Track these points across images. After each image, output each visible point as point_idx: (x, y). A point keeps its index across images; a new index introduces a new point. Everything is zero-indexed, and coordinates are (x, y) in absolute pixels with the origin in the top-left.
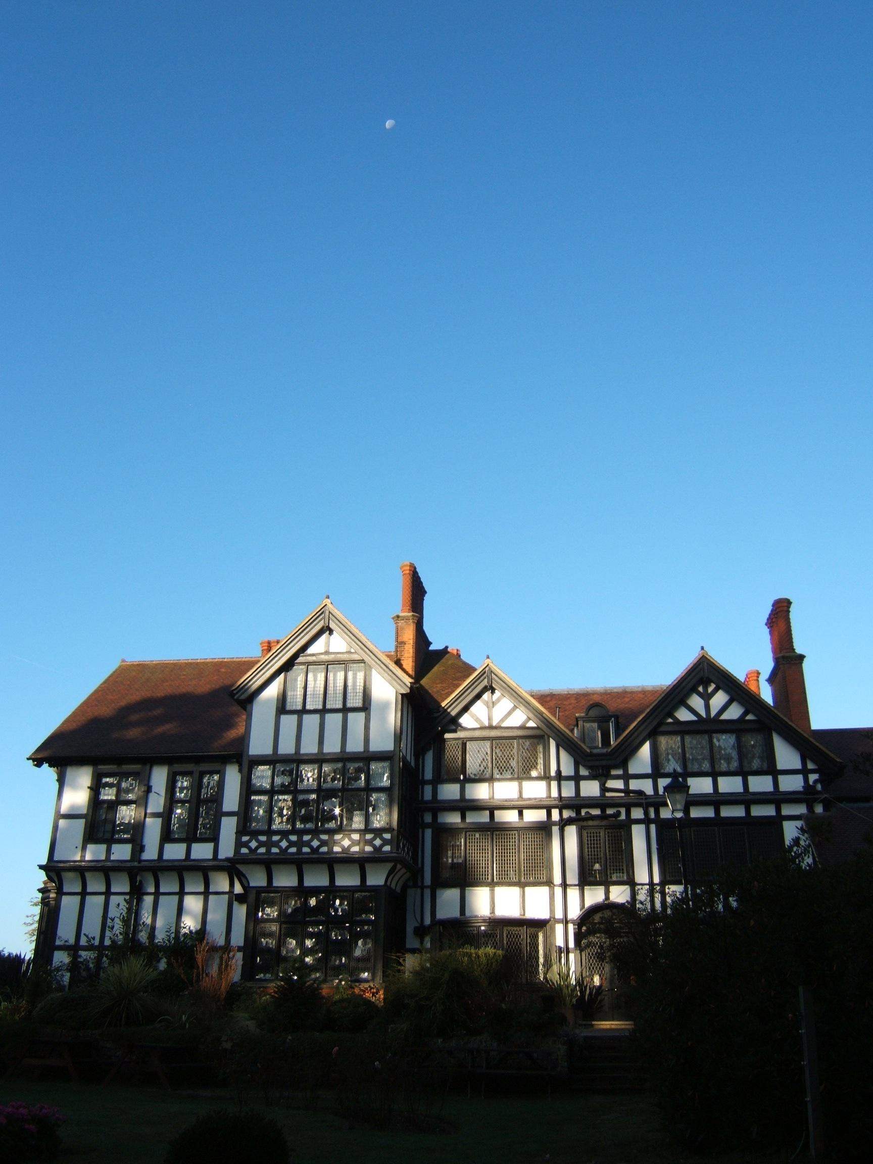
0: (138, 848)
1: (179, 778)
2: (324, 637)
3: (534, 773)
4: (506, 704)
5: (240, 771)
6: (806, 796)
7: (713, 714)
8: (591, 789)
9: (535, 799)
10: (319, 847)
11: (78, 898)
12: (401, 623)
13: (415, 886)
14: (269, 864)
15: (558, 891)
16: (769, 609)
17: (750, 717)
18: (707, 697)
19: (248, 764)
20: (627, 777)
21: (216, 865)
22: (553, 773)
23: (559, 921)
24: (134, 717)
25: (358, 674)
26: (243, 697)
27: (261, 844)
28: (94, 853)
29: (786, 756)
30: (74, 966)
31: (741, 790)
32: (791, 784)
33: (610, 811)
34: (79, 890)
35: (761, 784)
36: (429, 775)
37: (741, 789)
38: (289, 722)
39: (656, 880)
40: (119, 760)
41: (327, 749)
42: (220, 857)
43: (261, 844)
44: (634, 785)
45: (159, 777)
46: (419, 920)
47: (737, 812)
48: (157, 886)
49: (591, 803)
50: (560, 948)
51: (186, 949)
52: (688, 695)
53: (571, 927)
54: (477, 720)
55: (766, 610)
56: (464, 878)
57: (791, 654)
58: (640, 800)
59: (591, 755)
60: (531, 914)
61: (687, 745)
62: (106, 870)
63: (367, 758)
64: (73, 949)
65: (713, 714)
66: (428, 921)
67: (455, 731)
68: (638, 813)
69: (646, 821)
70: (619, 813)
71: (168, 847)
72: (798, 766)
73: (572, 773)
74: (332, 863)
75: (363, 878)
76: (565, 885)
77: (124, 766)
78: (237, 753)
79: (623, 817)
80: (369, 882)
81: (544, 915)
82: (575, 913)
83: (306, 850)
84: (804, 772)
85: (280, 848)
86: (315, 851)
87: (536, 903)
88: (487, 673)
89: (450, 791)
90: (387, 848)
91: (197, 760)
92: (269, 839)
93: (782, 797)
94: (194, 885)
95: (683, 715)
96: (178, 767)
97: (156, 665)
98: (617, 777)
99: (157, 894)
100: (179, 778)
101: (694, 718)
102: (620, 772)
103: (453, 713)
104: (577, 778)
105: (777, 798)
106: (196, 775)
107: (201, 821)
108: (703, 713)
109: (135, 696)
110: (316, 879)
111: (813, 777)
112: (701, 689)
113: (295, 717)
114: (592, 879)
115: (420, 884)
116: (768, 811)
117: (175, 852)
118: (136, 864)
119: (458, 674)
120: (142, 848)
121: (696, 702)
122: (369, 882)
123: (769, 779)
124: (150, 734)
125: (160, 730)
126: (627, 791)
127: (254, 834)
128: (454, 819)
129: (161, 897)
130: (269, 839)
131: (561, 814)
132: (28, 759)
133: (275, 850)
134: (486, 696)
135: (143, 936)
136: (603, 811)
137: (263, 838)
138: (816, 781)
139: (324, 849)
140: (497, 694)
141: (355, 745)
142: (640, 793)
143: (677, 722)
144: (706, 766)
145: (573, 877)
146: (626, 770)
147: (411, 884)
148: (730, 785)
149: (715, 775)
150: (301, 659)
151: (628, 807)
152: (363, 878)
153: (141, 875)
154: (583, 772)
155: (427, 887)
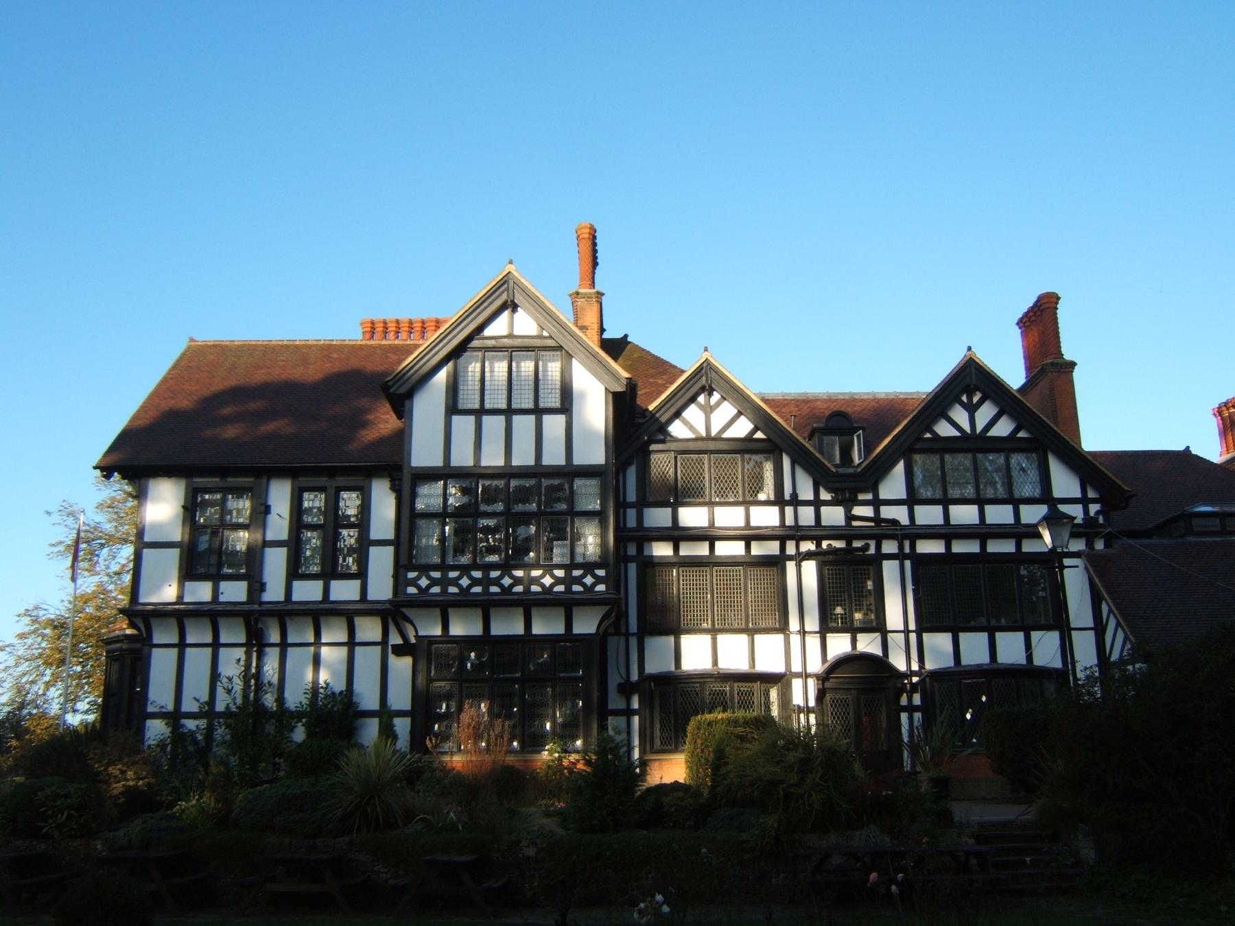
0: (258, 586)
1: (306, 495)
3: (762, 497)
4: (727, 410)
5: (393, 488)
6: (1087, 530)
7: (979, 429)
8: (834, 515)
9: (766, 527)
10: (512, 586)
11: (209, 650)
12: (581, 302)
13: (617, 633)
14: (444, 608)
15: (795, 640)
16: (1029, 302)
17: (1022, 434)
18: (972, 409)
19: (407, 481)
21: (366, 608)
22: (787, 497)
23: (798, 675)
24: (227, 411)
25: (496, 365)
26: (402, 390)
27: (434, 582)
28: (201, 592)
30: (179, 736)
31: (941, 522)
33: (857, 544)
36: (632, 496)
38: (463, 426)
39: (912, 626)
40: (223, 472)
41: (547, 461)
42: (370, 598)
43: (434, 582)
44: (887, 512)
45: (280, 495)
46: (624, 674)
47: (972, 547)
48: (284, 635)
49: (834, 533)
50: (799, 707)
51: (335, 715)
52: (949, 406)
53: (811, 683)
54: (691, 428)
55: (1027, 302)
56: (666, 621)
57: (1060, 361)
58: (890, 529)
60: (762, 667)
61: (948, 467)
62: (213, 614)
63: (571, 472)
64: (174, 717)
65: (979, 429)
66: (635, 677)
67: (663, 442)
68: (889, 547)
69: (900, 556)
70: (867, 547)
71: (297, 585)
72: (1077, 494)
74: (529, 604)
75: (569, 625)
76: (803, 632)
77: (229, 479)
78: (391, 462)
79: (872, 551)
80: (577, 630)
81: (779, 668)
82: (815, 665)
83: (494, 589)
84: (1084, 501)
85: (459, 586)
86: (507, 590)
87: (769, 654)
88: (705, 369)
89: (658, 517)
90: (601, 588)
91: (332, 472)
92: (486, 575)
93: (1025, 530)
94: (334, 633)
95: (944, 429)
96: (305, 481)
97: (239, 346)
98: (865, 503)
99: (284, 645)
100: (306, 495)
101: (957, 434)
102: (869, 496)
103: (663, 419)
104: (817, 503)
106: (332, 491)
107: (328, 548)
108: (967, 428)
109: (220, 384)
110: (508, 626)
111: (1094, 508)
112: (964, 398)
113: (472, 418)
114: (834, 625)
115: (623, 631)
117: (308, 591)
118: (256, 607)
119: (652, 371)
120: (262, 587)
121: (960, 415)
122: (577, 630)
124: (244, 436)
125: (269, 427)
126: (877, 519)
127: (425, 569)
128: (662, 550)
129: (289, 649)
131: (797, 547)
132: (95, 468)
133: (453, 589)
134: (701, 399)
135: (269, 700)
136: (849, 543)
137: (436, 575)
138: (1097, 513)
139: (519, 589)
140: (716, 396)
141: (554, 456)
142: (895, 522)
143: (937, 437)
144: (969, 491)
145: (812, 624)
146: (876, 494)
147: (612, 630)
149: (946, 502)
150: (475, 343)
152: (569, 625)
153: (259, 622)
154: (825, 495)
155: (633, 634)
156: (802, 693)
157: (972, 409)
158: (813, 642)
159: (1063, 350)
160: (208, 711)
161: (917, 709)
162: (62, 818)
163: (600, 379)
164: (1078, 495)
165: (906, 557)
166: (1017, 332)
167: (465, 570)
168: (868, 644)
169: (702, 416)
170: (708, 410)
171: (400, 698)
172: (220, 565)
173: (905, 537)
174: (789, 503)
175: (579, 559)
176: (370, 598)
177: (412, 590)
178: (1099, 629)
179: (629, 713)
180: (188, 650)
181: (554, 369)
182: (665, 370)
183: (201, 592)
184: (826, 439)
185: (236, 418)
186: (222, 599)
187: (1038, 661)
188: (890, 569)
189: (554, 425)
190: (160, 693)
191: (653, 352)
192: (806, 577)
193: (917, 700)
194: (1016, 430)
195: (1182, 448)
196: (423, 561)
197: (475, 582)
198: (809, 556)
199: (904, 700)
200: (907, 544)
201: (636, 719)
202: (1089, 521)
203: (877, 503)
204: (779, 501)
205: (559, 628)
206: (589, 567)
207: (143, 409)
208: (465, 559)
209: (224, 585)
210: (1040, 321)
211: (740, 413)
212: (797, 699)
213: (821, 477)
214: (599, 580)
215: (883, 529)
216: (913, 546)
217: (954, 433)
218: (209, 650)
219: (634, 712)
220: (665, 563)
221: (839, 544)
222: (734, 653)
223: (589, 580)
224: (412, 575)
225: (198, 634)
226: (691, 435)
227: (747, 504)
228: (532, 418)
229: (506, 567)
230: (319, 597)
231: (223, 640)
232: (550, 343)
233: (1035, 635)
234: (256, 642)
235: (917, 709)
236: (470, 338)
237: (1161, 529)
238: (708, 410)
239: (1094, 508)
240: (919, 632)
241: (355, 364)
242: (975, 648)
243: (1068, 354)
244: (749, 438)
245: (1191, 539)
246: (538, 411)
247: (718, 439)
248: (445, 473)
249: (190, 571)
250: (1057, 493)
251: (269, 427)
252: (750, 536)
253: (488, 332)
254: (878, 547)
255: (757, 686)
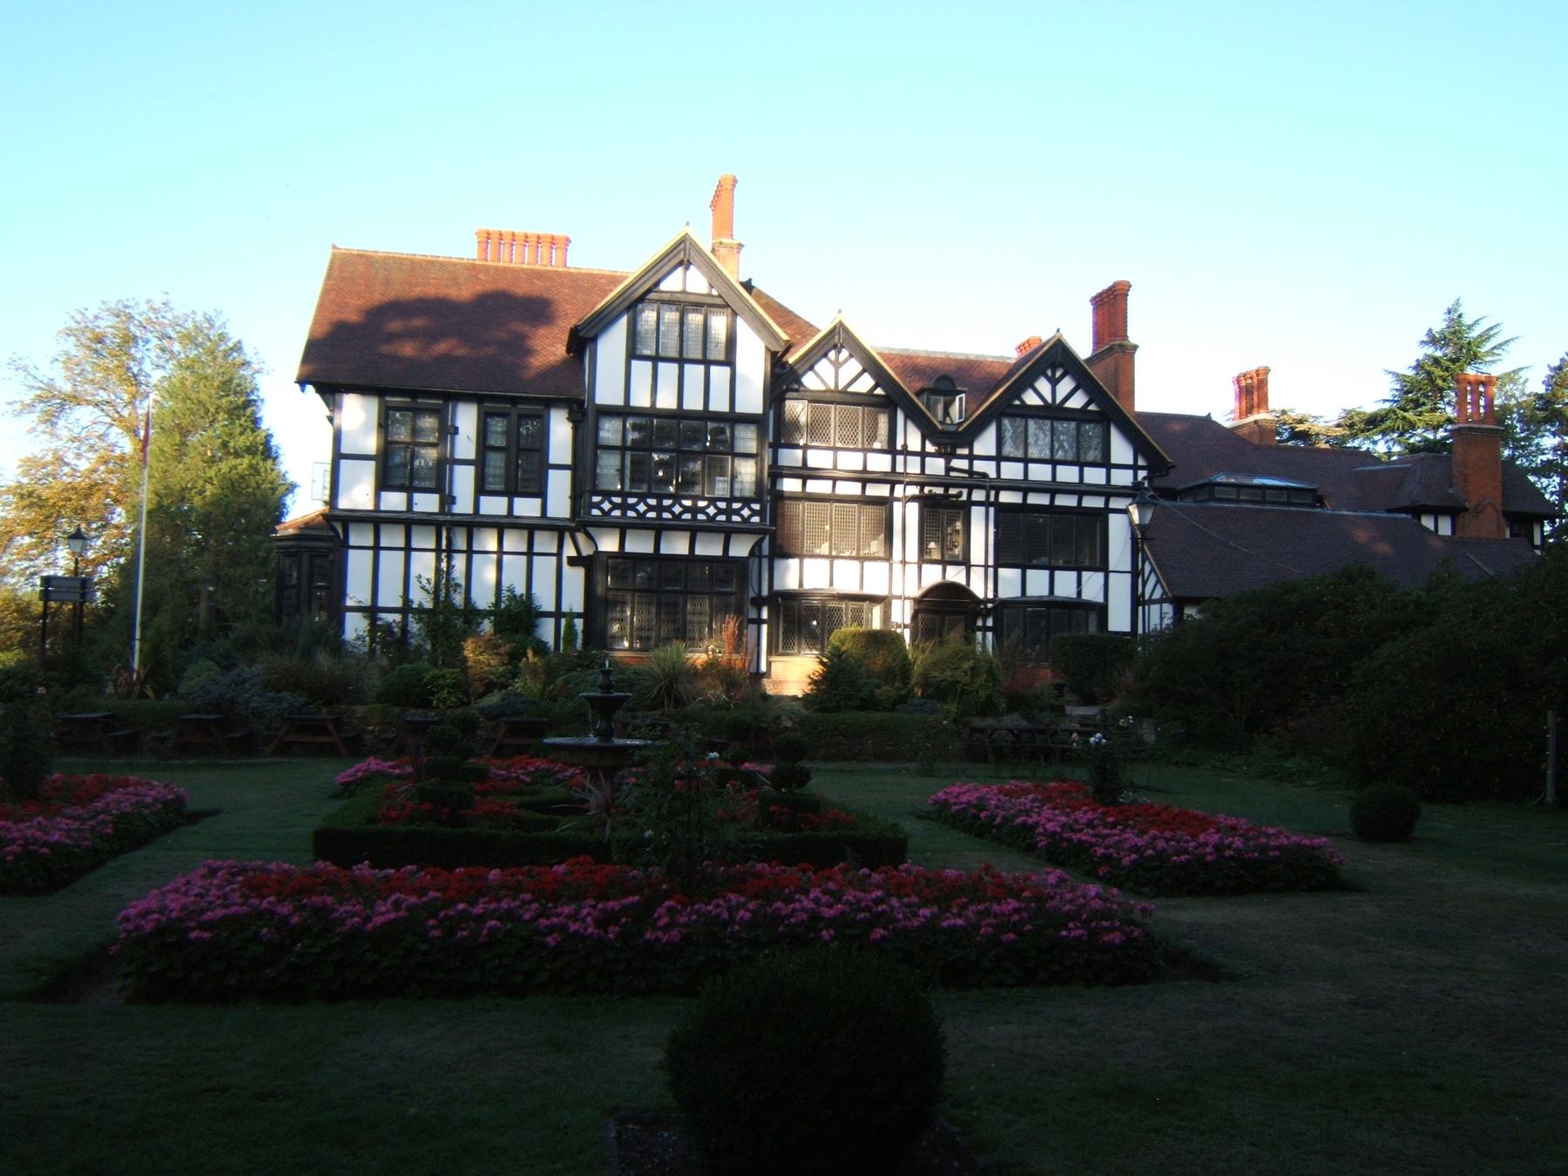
2: (681, 269)
8: (936, 466)
15: (897, 567)
18: (1054, 382)
19: (585, 415)
20: (971, 458)
21: (544, 524)
28: (394, 501)
29: (1121, 450)
32: (1122, 478)
33: (952, 491)
34: (371, 543)
35: (1095, 476)
37: (1103, 482)
39: (991, 562)
40: (414, 394)
44: (979, 466)
45: (466, 419)
47: (1043, 500)
49: (935, 481)
52: (1036, 378)
59: (943, 433)
62: (409, 522)
63: (734, 418)
64: (372, 611)
66: (765, 592)
68: (978, 495)
69: (986, 504)
70: (960, 494)
71: (483, 499)
73: (918, 449)
79: (964, 498)
80: (732, 553)
81: (881, 591)
83: (666, 515)
84: (1135, 468)
87: (875, 579)
90: (756, 519)
92: (625, 501)
95: (1031, 399)
98: (962, 457)
102: (965, 451)
105: (1108, 491)
106: (514, 418)
107: (520, 469)
108: (1049, 400)
110: (677, 545)
111: (1142, 474)
116: (1095, 502)
117: (494, 506)
120: (453, 500)
121: (1043, 385)
123: (1103, 471)
125: (442, 347)
126: (970, 472)
127: (607, 495)
130: (729, 505)
134: (832, 355)
135: (458, 599)
136: (946, 491)
137: (617, 500)
140: (845, 353)
141: (719, 404)
142: (984, 475)
143: (1024, 405)
146: (971, 450)
148: (1068, 474)
150: (652, 296)
151: (971, 488)
154: (930, 448)
156: (902, 614)
157: (1054, 382)
158: (912, 570)
159: (1129, 333)
160: (406, 608)
161: (989, 629)
162: (445, 694)
163: (763, 339)
164: (1131, 462)
165: (991, 504)
166: (1090, 308)
167: (642, 498)
168: (955, 575)
169: (832, 370)
170: (837, 365)
171: (574, 599)
172: (412, 478)
173: (993, 488)
174: (901, 453)
175: (737, 494)
176: (549, 514)
177: (596, 512)
178: (1136, 573)
179: (759, 622)
180: (382, 553)
181: (719, 324)
182: (806, 329)
183: (394, 501)
184: (933, 398)
185: (411, 335)
186: (416, 509)
187: (1086, 596)
188: (977, 513)
189: (720, 374)
190: (357, 591)
191: (778, 299)
192: (908, 516)
193: (990, 623)
194: (1088, 404)
195: (1204, 414)
196: (605, 487)
197: (650, 508)
198: (913, 499)
199: (980, 623)
200: (993, 493)
201: (765, 628)
202: (1137, 485)
203: (971, 458)
204: (891, 450)
205: (717, 551)
206: (746, 502)
207: (316, 322)
208: (644, 489)
209: (417, 497)
210: (1110, 306)
211: (864, 371)
212: (896, 617)
213: (928, 431)
214: (754, 513)
215: (975, 480)
216: (997, 496)
217: (1038, 402)
218: (402, 554)
219: (764, 622)
220: (796, 498)
221: (939, 491)
222: (847, 578)
223: (746, 512)
224: (596, 499)
225: (393, 537)
226: (822, 388)
227: (865, 451)
228: (701, 368)
229: (677, 498)
230: (505, 512)
231: (414, 545)
232: (719, 301)
233: (1085, 575)
234: (445, 551)
235: (989, 629)
236: (649, 291)
237: (1190, 492)
238: (837, 365)
239: (1142, 474)
240: (996, 567)
241: (503, 285)
242: (1038, 583)
243: (1133, 336)
244: (870, 393)
245: (1213, 504)
246: (707, 363)
247: (844, 392)
248: (623, 412)
249: (384, 483)
250: (1116, 458)
251: (442, 347)
252: (865, 478)
253: (663, 286)
254: (969, 495)
255: (866, 604)
